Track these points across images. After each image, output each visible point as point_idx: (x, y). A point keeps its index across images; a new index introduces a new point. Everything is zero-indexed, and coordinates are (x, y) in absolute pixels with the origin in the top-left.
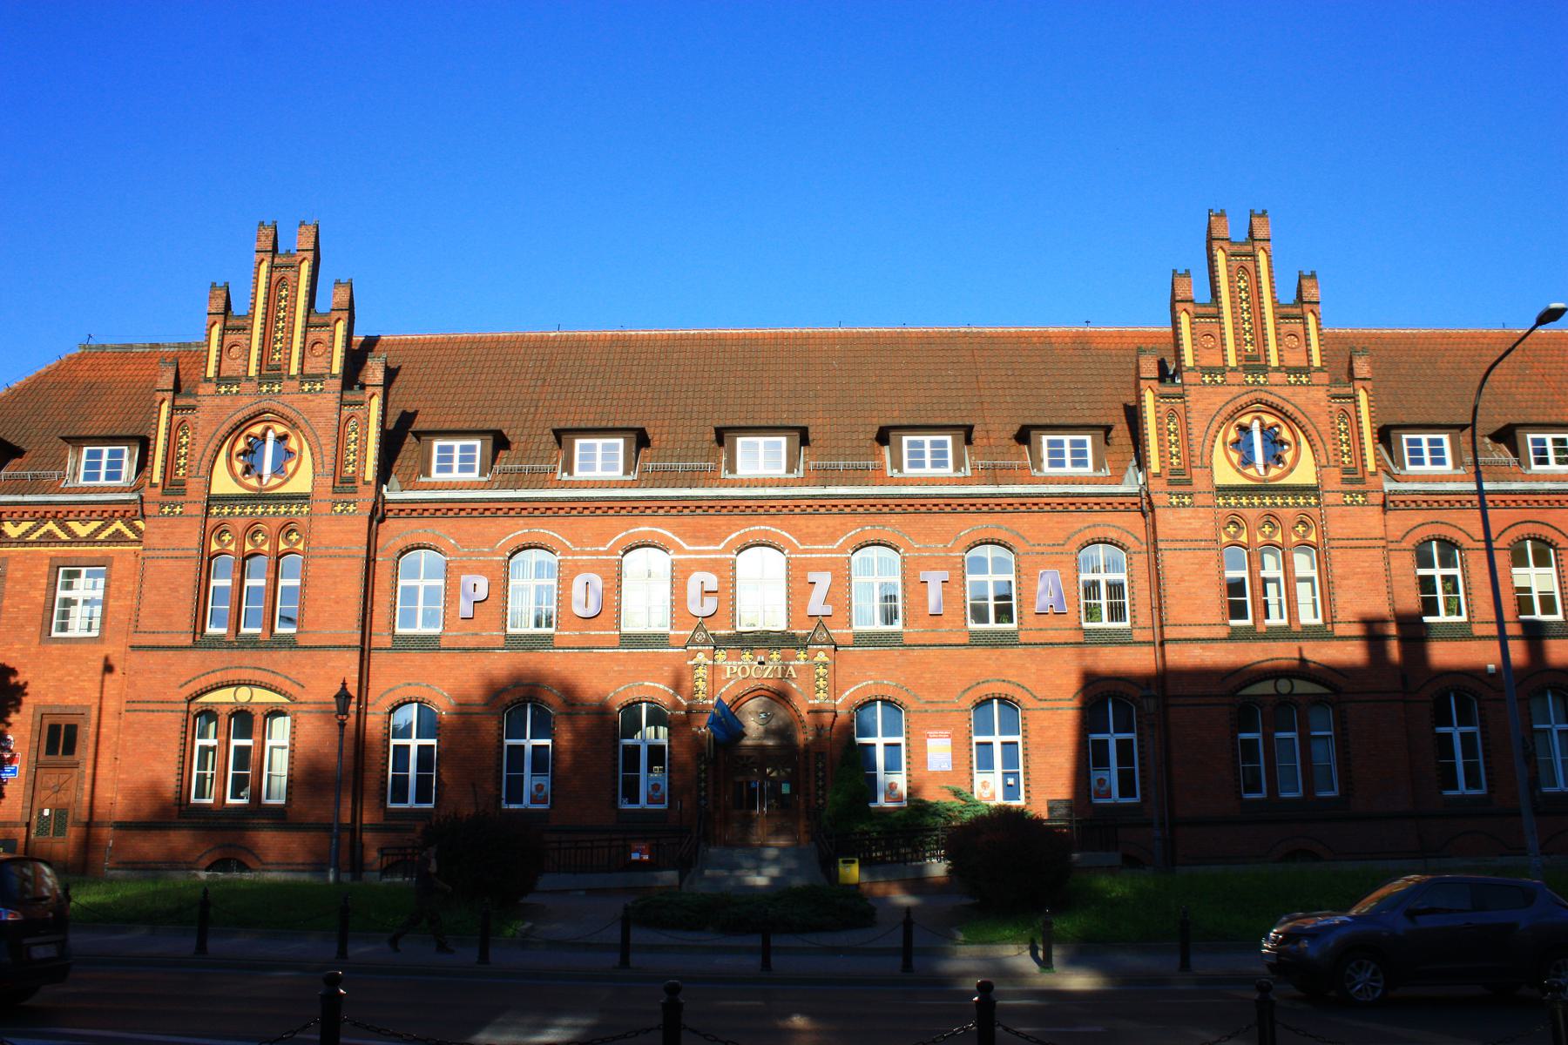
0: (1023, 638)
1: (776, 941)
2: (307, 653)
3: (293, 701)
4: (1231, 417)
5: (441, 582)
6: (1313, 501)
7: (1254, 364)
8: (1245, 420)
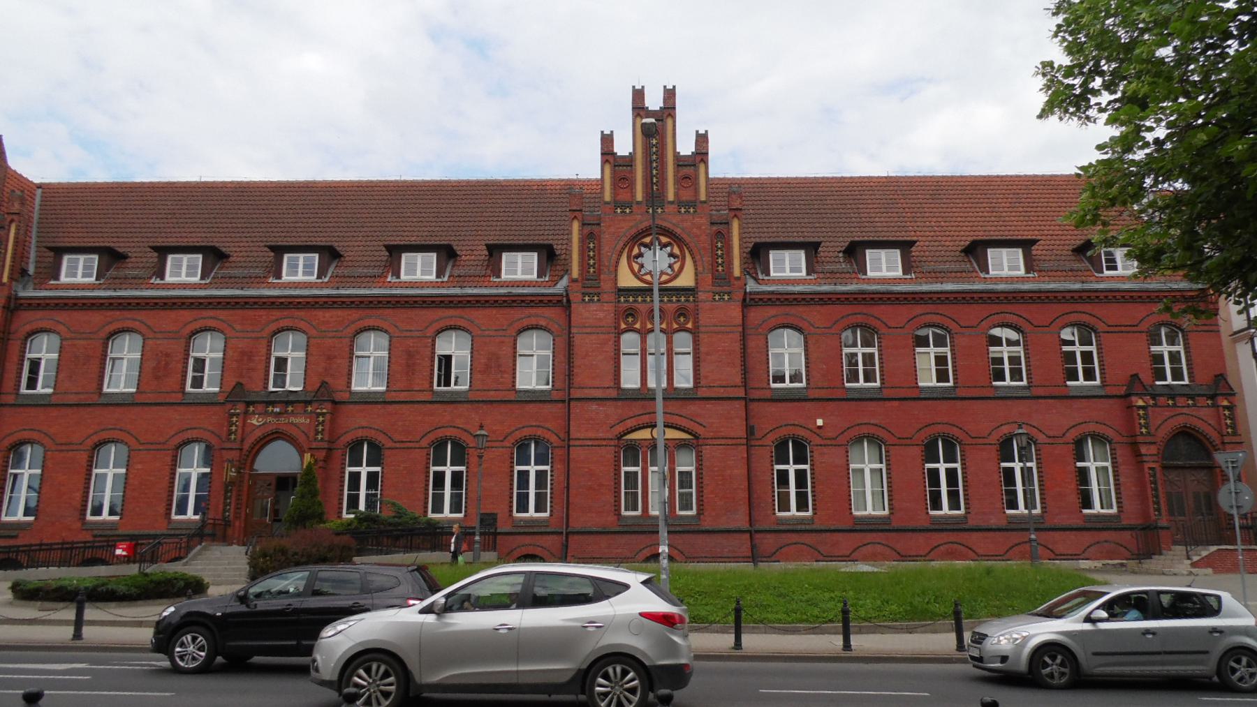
1: (90, 613)
3: (696, 437)
5: (386, 354)
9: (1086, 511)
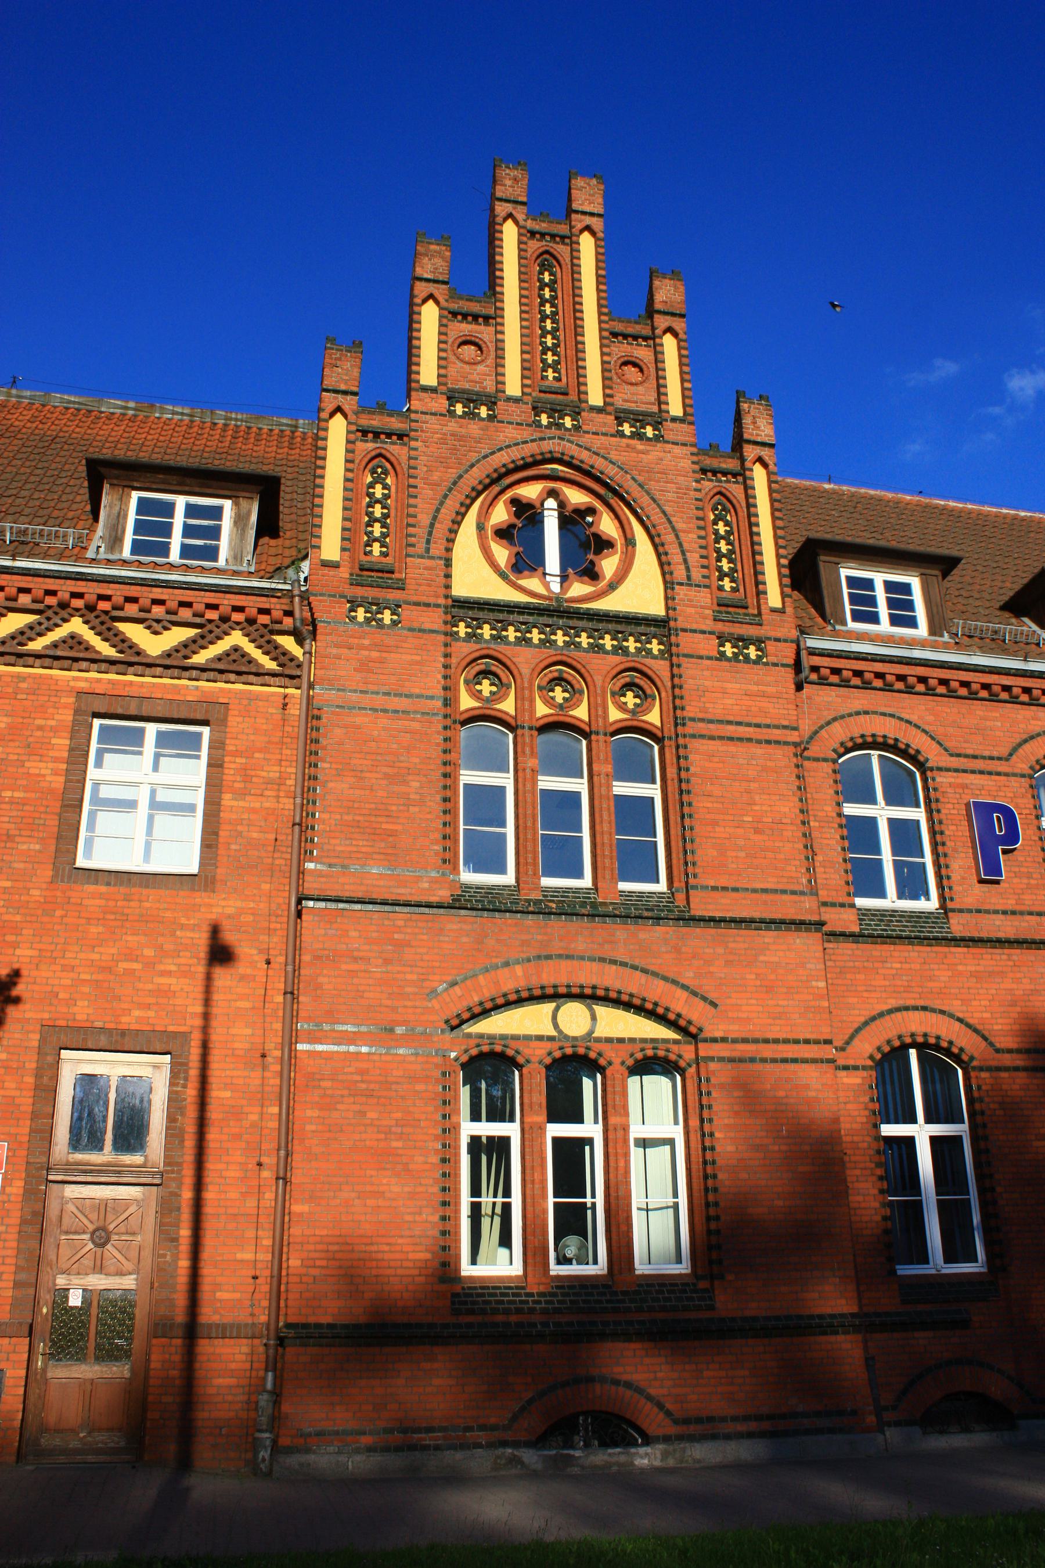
0: (958, 926)
2: (712, 932)
6: (655, 647)
8: (530, 492)
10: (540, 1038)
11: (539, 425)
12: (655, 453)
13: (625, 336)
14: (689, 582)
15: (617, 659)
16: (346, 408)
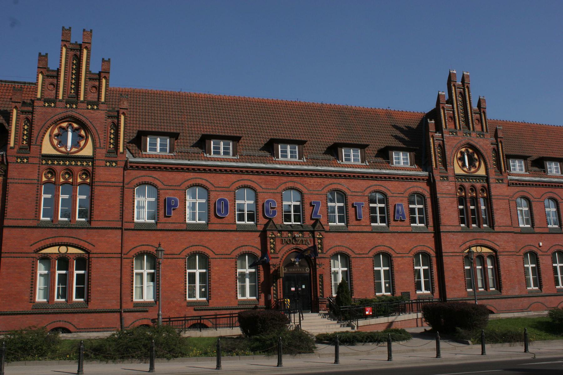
4: (56, 123)
7: (73, 100)
9: (557, 287)
10: (55, 253)
11: (66, 107)
12: (97, 113)
13: (93, 79)
14: (100, 147)
15: (81, 167)
16: (18, 106)
